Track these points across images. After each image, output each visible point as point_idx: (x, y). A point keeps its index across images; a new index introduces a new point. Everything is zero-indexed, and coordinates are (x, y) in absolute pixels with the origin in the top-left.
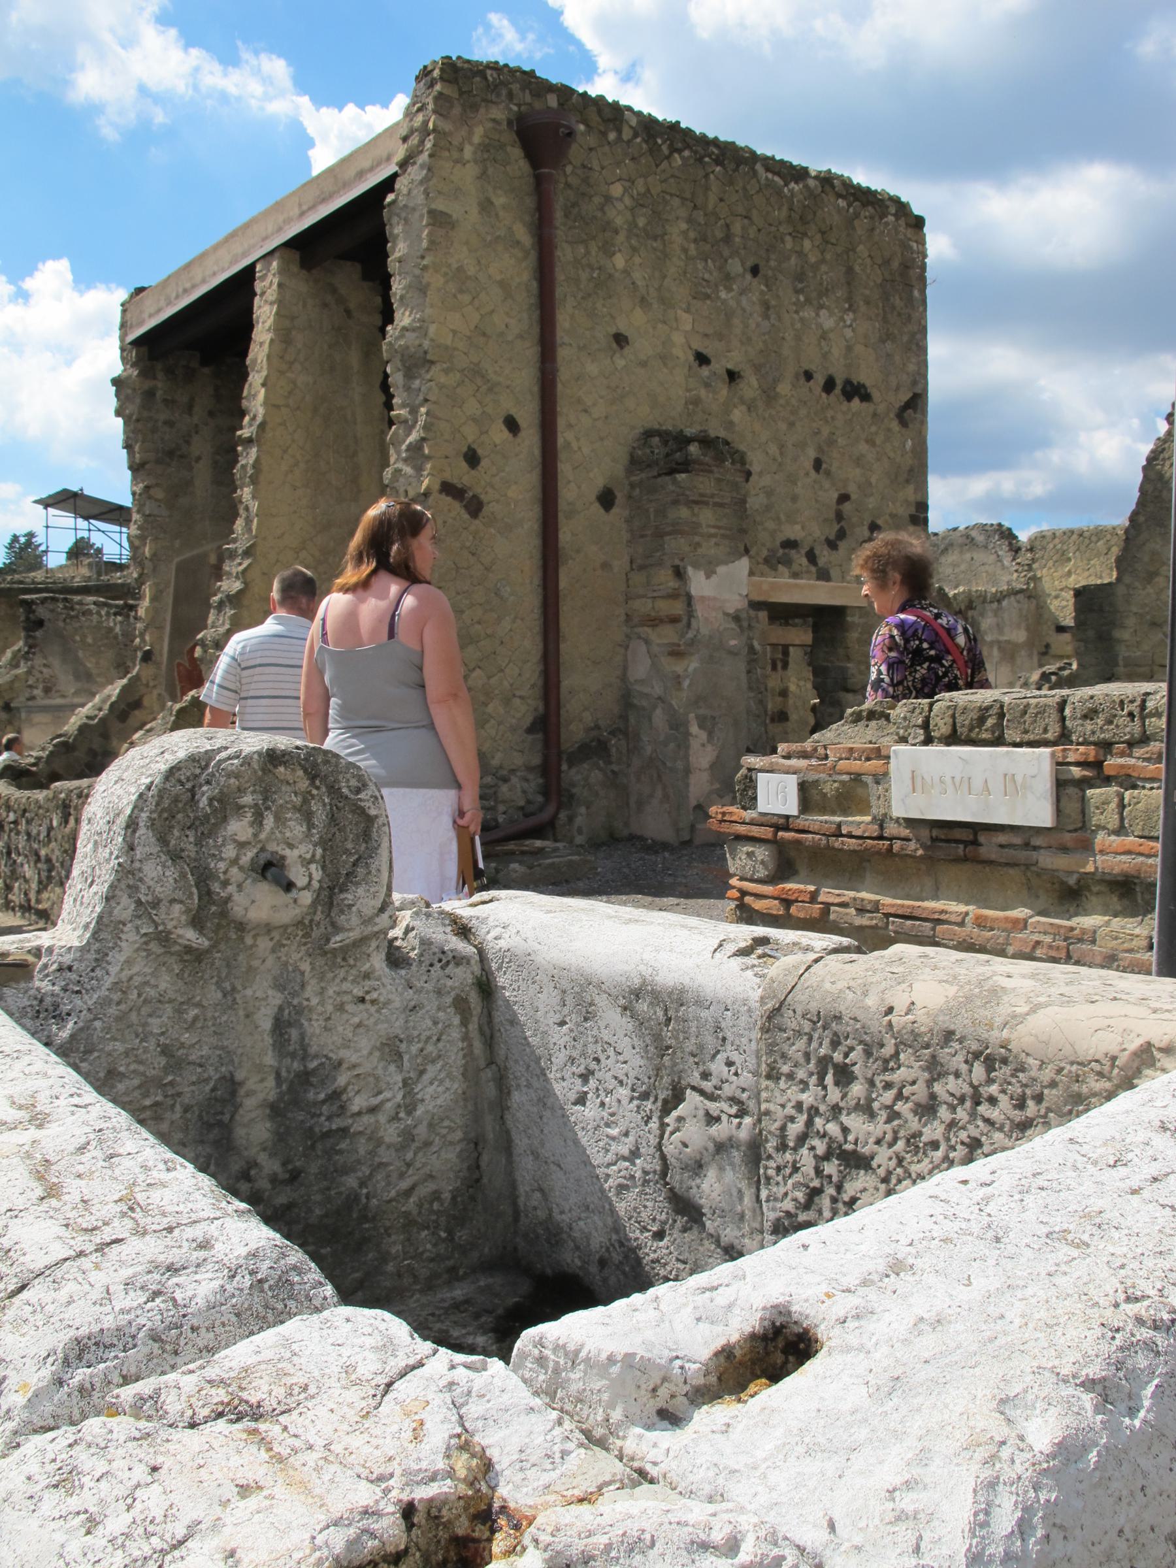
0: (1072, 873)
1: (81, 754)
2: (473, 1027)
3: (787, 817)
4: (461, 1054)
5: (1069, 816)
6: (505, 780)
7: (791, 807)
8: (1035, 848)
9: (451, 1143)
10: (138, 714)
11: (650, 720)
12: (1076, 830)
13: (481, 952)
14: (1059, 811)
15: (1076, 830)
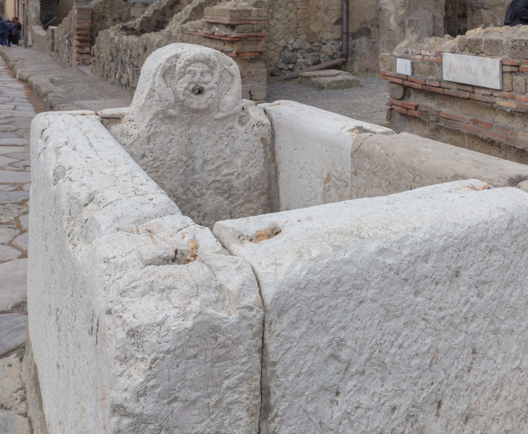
0: (509, 108)
1: (153, 22)
2: (268, 149)
3: (407, 76)
4: (263, 157)
5: (507, 86)
6: (325, 44)
7: (409, 72)
8: (495, 97)
9: (258, 189)
10: (179, 6)
11: (389, 20)
12: (509, 91)
13: (271, 120)
14: (502, 83)
15: (509, 91)
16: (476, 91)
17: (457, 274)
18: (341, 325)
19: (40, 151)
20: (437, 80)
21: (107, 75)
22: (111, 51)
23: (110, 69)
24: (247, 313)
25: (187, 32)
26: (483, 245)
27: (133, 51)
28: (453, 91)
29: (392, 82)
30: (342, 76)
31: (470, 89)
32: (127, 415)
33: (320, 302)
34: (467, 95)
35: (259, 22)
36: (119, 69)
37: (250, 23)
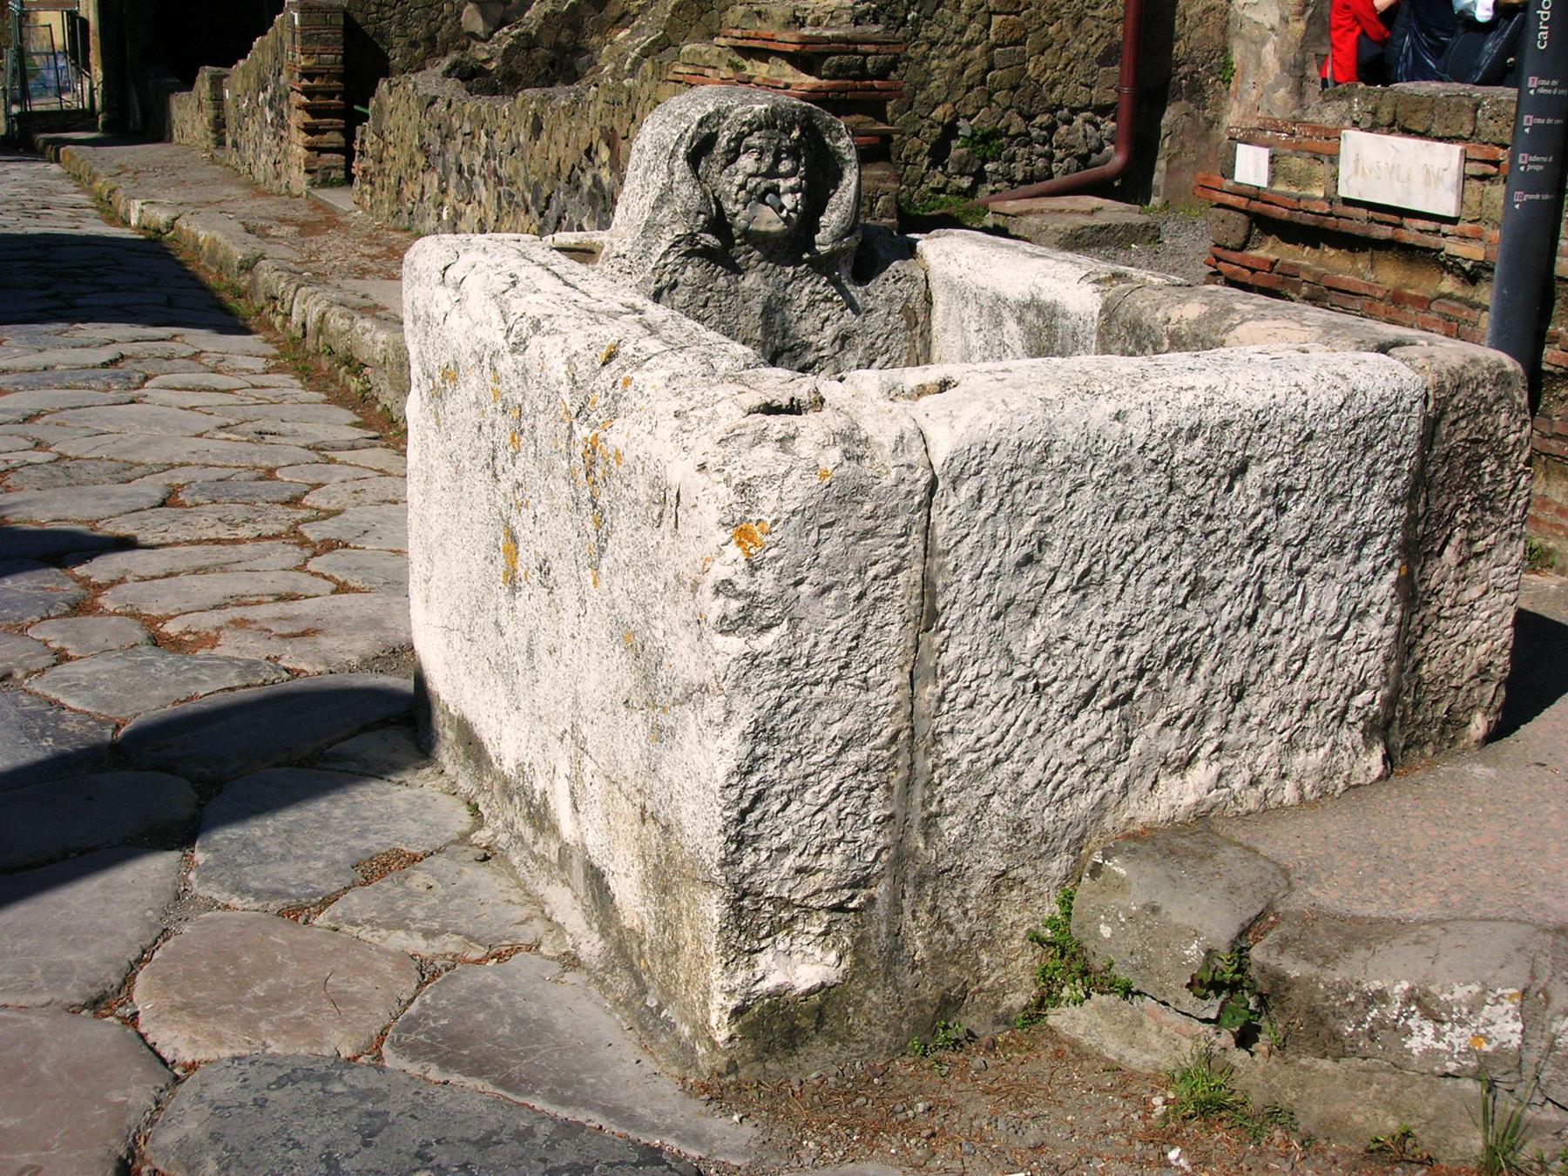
8: (1445, 235)
14: (1462, 202)
16: (1406, 221)
17: (1243, 469)
18: (1047, 514)
19: (447, 309)
20: (1325, 198)
21: (411, 213)
22: (421, 137)
23: (423, 193)
24: (906, 474)
25: (670, 77)
26: (1295, 427)
27: (498, 136)
28: (1358, 222)
29: (1220, 206)
30: (1114, 212)
31: (1394, 219)
32: (738, 596)
33: (1017, 475)
34: (1384, 232)
35: (884, 49)
36: (452, 191)
37: (855, 52)
